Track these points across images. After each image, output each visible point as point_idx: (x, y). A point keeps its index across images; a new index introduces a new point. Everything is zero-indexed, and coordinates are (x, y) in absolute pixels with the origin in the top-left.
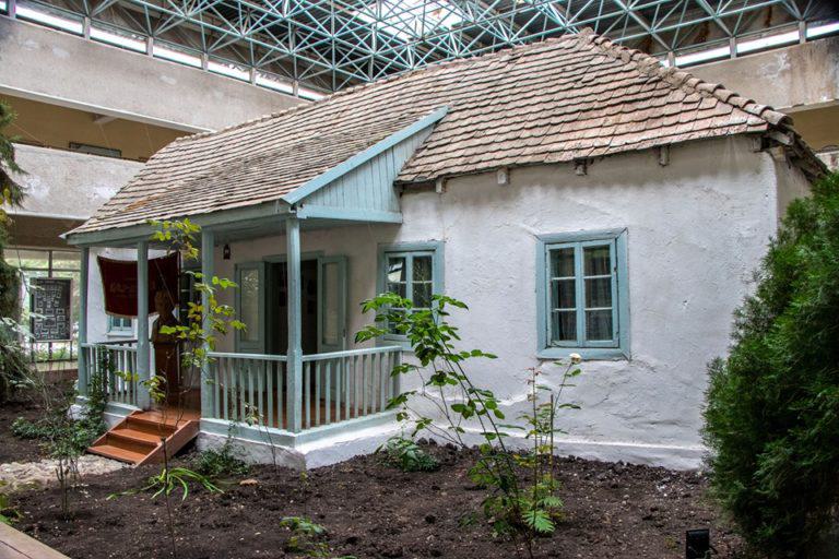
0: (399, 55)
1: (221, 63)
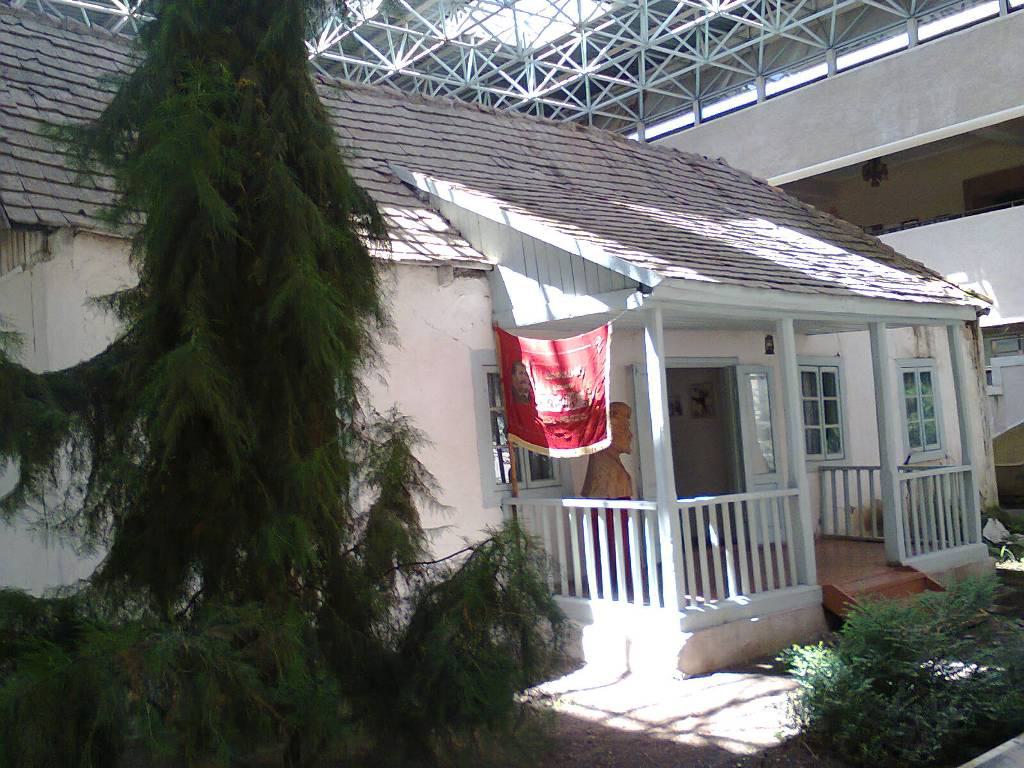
0: (626, 27)
1: (1010, 206)
